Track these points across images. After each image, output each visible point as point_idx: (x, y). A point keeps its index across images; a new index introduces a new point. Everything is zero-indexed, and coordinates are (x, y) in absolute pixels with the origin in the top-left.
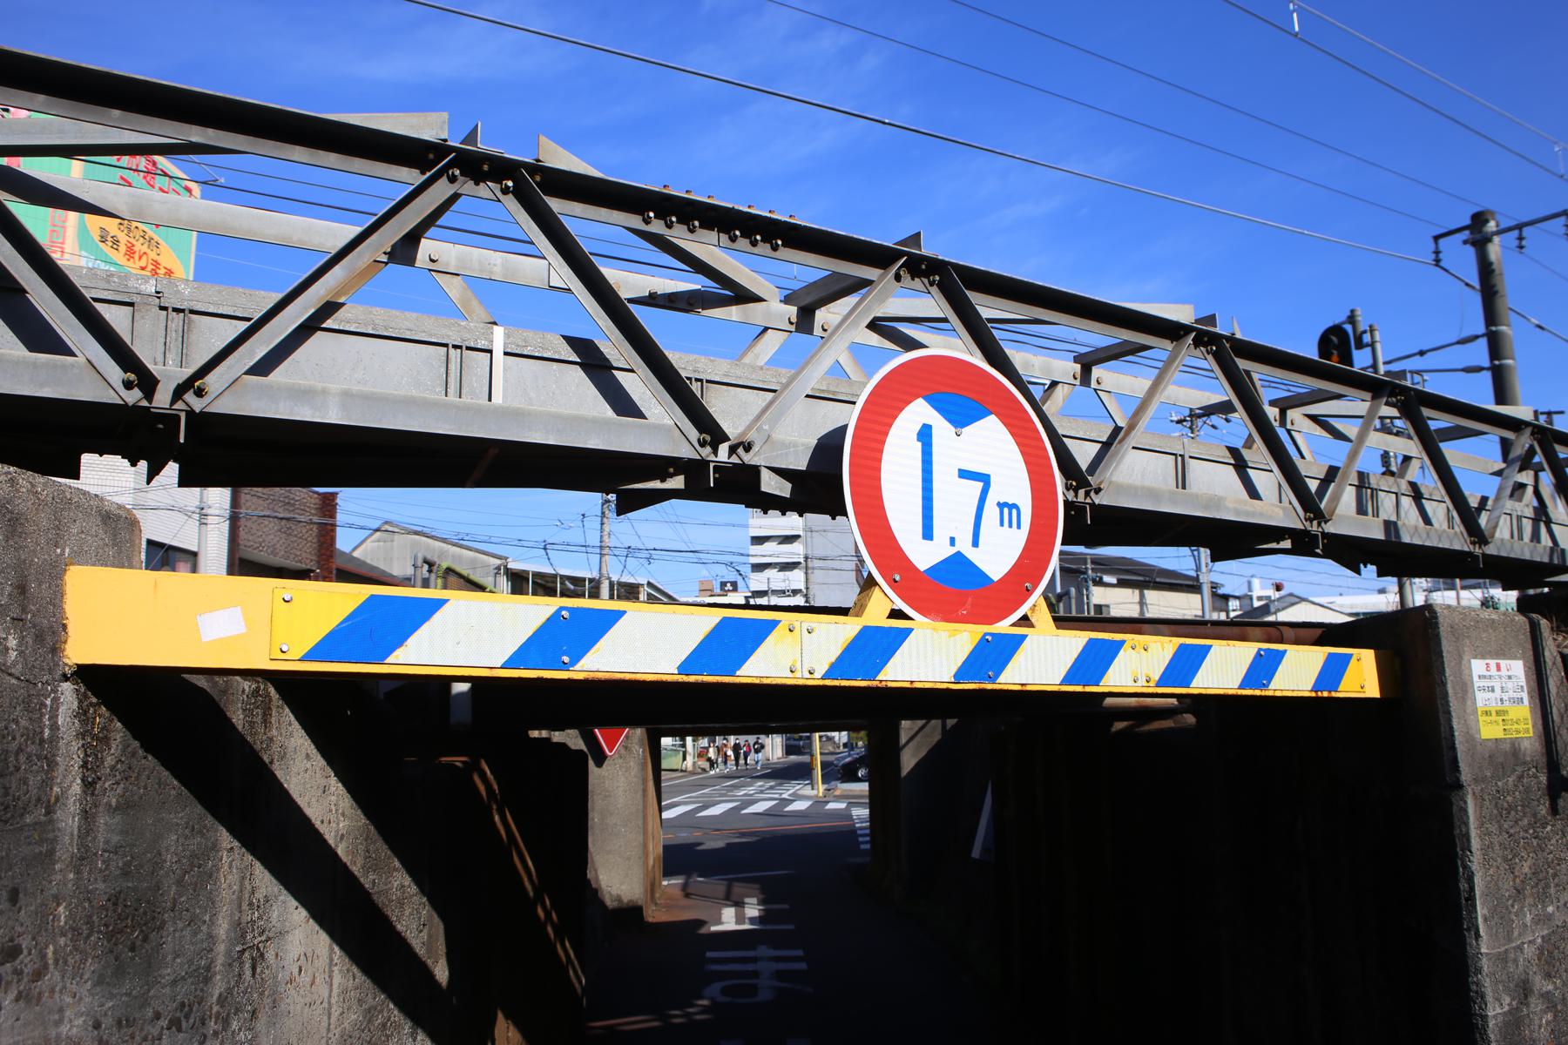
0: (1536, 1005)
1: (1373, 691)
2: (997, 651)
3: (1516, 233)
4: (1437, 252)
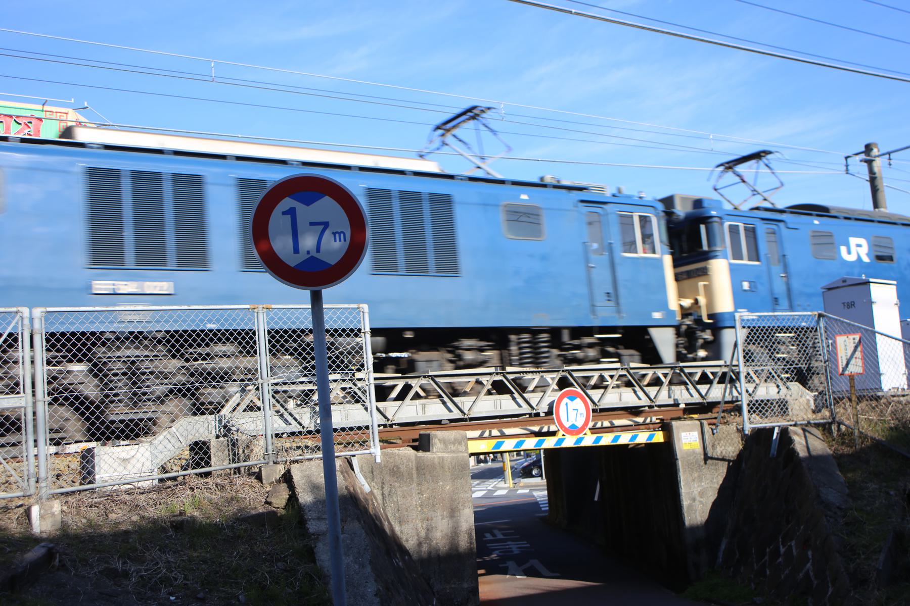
0: (697, 503)
2: (581, 439)
3: (887, 156)
4: (847, 166)
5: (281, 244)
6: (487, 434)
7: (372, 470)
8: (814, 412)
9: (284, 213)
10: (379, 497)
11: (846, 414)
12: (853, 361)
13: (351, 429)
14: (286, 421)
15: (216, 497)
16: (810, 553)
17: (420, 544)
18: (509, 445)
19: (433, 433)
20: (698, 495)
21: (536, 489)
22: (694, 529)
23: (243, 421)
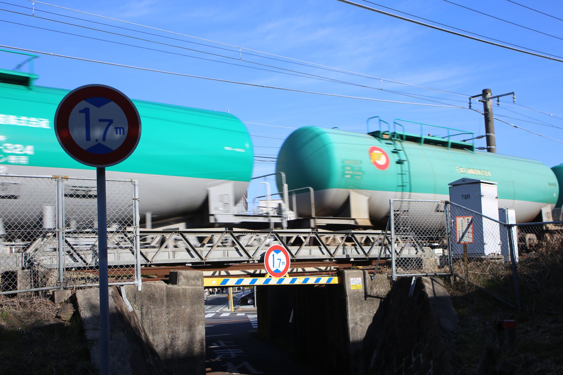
0: (358, 326)
1: (337, 282)
2: (281, 280)
3: (497, 99)
4: (470, 103)
5: (77, 134)
6: (217, 274)
7: (135, 296)
8: (439, 267)
9: (81, 112)
10: (139, 316)
11: (460, 269)
12: (466, 235)
13: (121, 266)
14: (75, 260)
15: (20, 311)
16: (432, 362)
17: (166, 349)
18: (232, 282)
19: (180, 271)
20: (359, 320)
21: (249, 313)
22: (356, 343)
23: (43, 258)
